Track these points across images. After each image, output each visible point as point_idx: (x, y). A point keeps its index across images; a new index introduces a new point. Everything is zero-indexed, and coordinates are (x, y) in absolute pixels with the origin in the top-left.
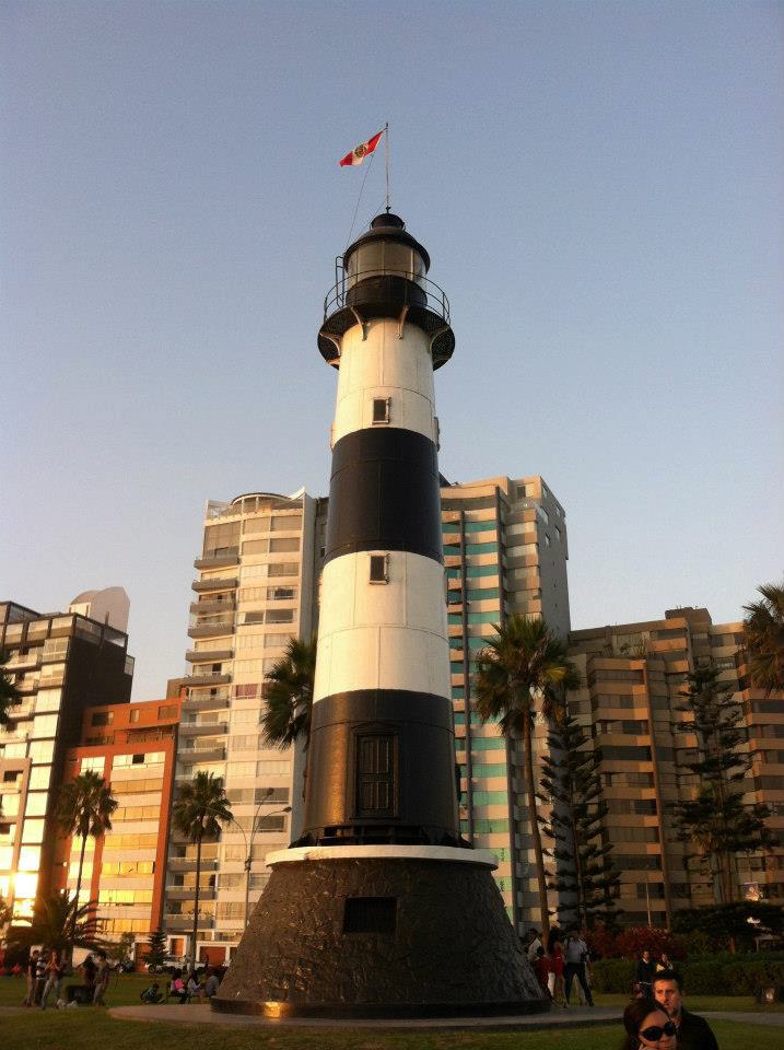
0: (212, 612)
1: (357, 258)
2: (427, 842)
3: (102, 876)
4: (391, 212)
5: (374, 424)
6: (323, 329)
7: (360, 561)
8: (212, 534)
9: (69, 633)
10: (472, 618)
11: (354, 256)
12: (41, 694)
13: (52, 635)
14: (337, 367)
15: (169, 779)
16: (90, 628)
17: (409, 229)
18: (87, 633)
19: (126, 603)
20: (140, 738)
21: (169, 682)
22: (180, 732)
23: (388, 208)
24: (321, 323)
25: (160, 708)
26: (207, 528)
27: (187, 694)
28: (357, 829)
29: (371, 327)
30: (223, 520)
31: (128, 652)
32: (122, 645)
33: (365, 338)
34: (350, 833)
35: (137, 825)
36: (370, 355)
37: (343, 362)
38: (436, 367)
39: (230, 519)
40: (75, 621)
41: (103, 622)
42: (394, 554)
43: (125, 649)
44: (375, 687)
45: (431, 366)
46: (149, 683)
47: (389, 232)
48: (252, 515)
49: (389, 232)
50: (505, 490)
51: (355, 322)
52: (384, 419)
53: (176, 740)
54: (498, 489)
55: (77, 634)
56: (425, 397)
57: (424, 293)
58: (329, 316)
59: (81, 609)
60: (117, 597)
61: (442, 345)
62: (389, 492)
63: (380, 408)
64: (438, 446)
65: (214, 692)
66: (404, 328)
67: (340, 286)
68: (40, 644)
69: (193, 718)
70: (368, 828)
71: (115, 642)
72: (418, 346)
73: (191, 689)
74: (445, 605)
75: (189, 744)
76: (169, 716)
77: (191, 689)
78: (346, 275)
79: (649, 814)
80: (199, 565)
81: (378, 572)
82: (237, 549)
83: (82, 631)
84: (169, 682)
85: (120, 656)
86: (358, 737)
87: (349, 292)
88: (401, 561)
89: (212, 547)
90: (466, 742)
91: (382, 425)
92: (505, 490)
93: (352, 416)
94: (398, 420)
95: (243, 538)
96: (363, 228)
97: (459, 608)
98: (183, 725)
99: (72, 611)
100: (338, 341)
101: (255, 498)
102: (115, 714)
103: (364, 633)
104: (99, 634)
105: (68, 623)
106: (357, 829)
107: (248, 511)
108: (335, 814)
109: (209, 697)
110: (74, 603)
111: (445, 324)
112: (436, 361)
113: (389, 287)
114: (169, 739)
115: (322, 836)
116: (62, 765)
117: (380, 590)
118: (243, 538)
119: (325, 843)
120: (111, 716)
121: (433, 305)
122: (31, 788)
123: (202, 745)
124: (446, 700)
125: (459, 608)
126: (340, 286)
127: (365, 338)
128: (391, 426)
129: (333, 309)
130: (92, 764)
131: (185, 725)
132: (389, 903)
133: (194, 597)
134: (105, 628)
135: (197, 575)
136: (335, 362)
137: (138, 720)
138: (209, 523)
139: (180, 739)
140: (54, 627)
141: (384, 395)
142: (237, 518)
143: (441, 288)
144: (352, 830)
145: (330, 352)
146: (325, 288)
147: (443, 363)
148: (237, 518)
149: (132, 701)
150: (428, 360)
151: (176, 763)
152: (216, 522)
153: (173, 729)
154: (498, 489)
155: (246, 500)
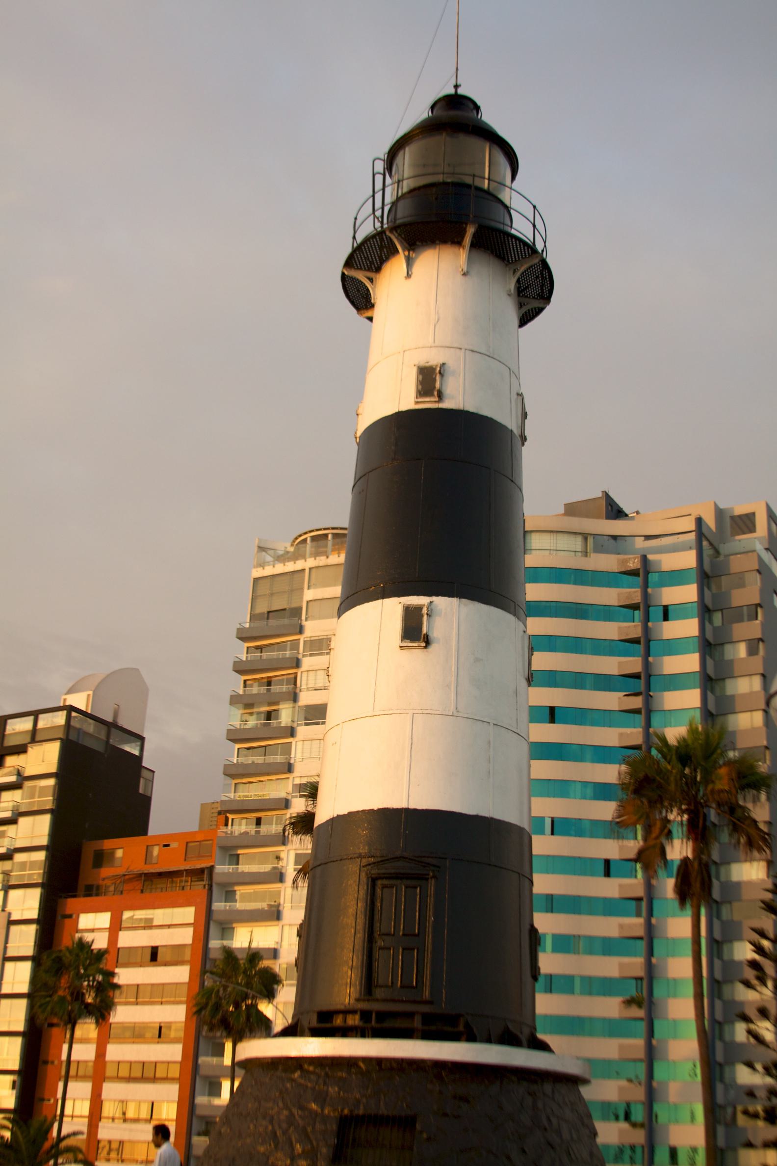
0: (261, 704)
1: (406, 160)
2: (471, 1038)
3: (383, 1110)
4: (461, 91)
5: (417, 403)
6: (349, 263)
7: (388, 612)
8: (263, 589)
9: (61, 735)
10: (656, 720)
11: (399, 160)
12: (22, 820)
13: (38, 738)
14: (370, 319)
15: (200, 945)
16: (90, 727)
17: (489, 116)
18: (86, 734)
19: (142, 692)
20: (155, 884)
21: (202, 805)
22: (216, 879)
23: (456, 87)
24: (348, 250)
25: (189, 843)
26: (256, 580)
27: (226, 825)
28: (365, 1015)
29: (416, 258)
30: (280, 568)
31: (145, 763)
32: (137, 753)
33: (409, 276)
34: (354, 1020)
35: (153, 1007)
36: (426, 304)
37: (378, 313)
38: (524, 320)
39: (290, 567)
40: (69, 718)
41: (109, 718)
42: (441, 602)
43: (139, 758)
44: (404, 805)
45: (516, 322)
46: (173, 810)
47: (455, 118)
48: (322, 561)
49: (455, 118)
50: (710, 521)
51: (394, 252)
52: (432, 395)
53: (211, 886)
54: (699, 521)
55: (73, 737)
56: (498, 362)
57: (507, 209)
58: (360, 238)
59: (79, 701)
60: (130, 680)
61: (534, 289)
62: (437, 506)
63: (429, 379)
64: (524, 439)
65: (258, 822)
66: (470, 260)
67: (378, 197)
68: (21, 750)
69: (235, 859)
70: (382, 1016)
71: (127, 748)
72: (497, 291)
73: (231, 816)
74: (524, 683)
75: (230, 896)
76: (200, 856)
77: (231, 816)
78: (388, 180)
79: (557, 975)
80: (243, 636)
81: (414, 631)
82: (296, 612)
83: (79, 730)
84: (202, 805)
85: (134, 766)
86: (373, 881)
87: (394, 204)
88: (448, 613)
89: (262, 608)
90: (644, 904)
91: (429, 403)
92: (710, 521)
93: (389, 392)
94: (457, 396)
95: (309, 594)
96: (420, 112)
97: (637, 702)
98: (220, 869)
99: (68, 703)
100: (371, 280)
101: (326, 535)
102: (123, 853)
103: (388, 717)
104: (103, 736)
105: (60, 719)
106: (365, 1015)
107: (316, 555)
108: (345, 991)
109: (252, 829)
110: (69, 692)
111: (534, 251)
112: (524, 309)
113: (450, 194)
114: (199, 888)
115: (314, 1023)
116: (50, 922)
117: (416, 655)
118: (309, 594)
119: (316, 1033)
120: (119, 853)
121: (521, 227)
122: (10, 953)
123: (246, 898)
124: (521, 830)
125: (637, 702)
126: (378, 197)
127: (409, 276)
128: (446, 405)
129: (366, 229)
130: (92, 924)
131: (222, 869)
132: (407, 1123)
133: (237, 684)
134: (112, 726)
135: (241, 650)
136: (369, 314)
137: (161, 860)
138: (258, 573)
139: (215, 889)
140: (41, 724)
141: (433, 358)
142: (299, 565)
143: (533, 201)
144: (357, 1017)
145: (361, 300)
146: (353, 196)
147: (539, 311)
148: (299, 565)
149: (151, 832)
150: (512, 315)
151: (209, 923)
152: (269, 571)
153: (204, 874)
154: (699, 521)
155: (314, 538)
